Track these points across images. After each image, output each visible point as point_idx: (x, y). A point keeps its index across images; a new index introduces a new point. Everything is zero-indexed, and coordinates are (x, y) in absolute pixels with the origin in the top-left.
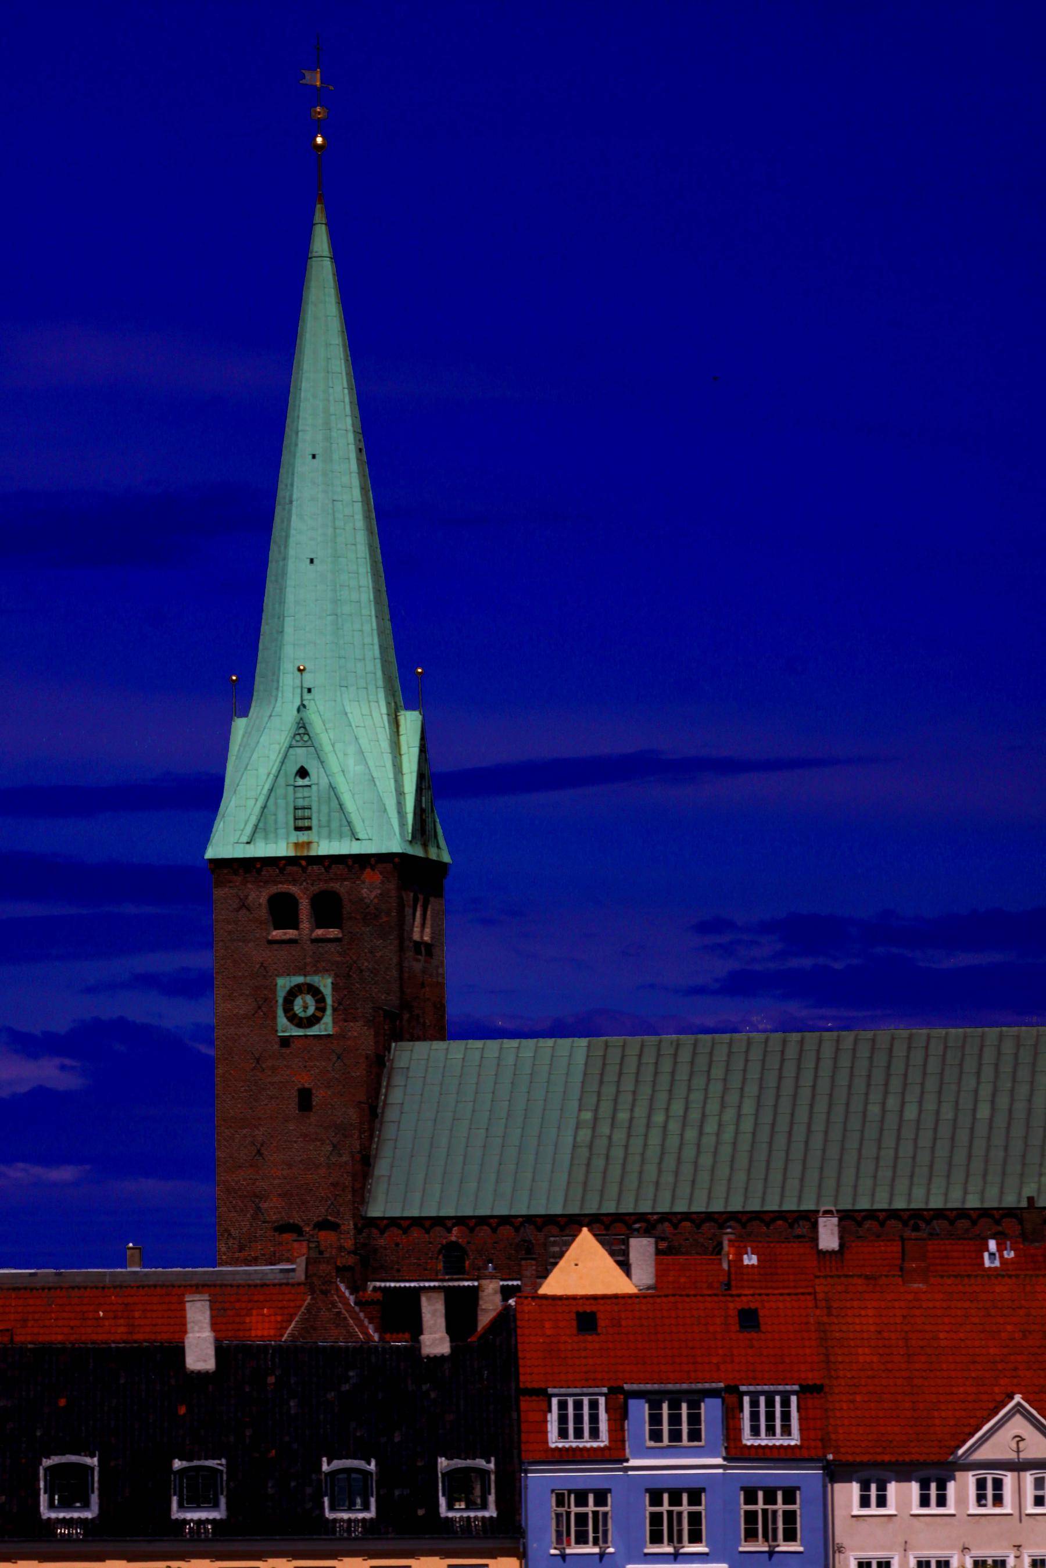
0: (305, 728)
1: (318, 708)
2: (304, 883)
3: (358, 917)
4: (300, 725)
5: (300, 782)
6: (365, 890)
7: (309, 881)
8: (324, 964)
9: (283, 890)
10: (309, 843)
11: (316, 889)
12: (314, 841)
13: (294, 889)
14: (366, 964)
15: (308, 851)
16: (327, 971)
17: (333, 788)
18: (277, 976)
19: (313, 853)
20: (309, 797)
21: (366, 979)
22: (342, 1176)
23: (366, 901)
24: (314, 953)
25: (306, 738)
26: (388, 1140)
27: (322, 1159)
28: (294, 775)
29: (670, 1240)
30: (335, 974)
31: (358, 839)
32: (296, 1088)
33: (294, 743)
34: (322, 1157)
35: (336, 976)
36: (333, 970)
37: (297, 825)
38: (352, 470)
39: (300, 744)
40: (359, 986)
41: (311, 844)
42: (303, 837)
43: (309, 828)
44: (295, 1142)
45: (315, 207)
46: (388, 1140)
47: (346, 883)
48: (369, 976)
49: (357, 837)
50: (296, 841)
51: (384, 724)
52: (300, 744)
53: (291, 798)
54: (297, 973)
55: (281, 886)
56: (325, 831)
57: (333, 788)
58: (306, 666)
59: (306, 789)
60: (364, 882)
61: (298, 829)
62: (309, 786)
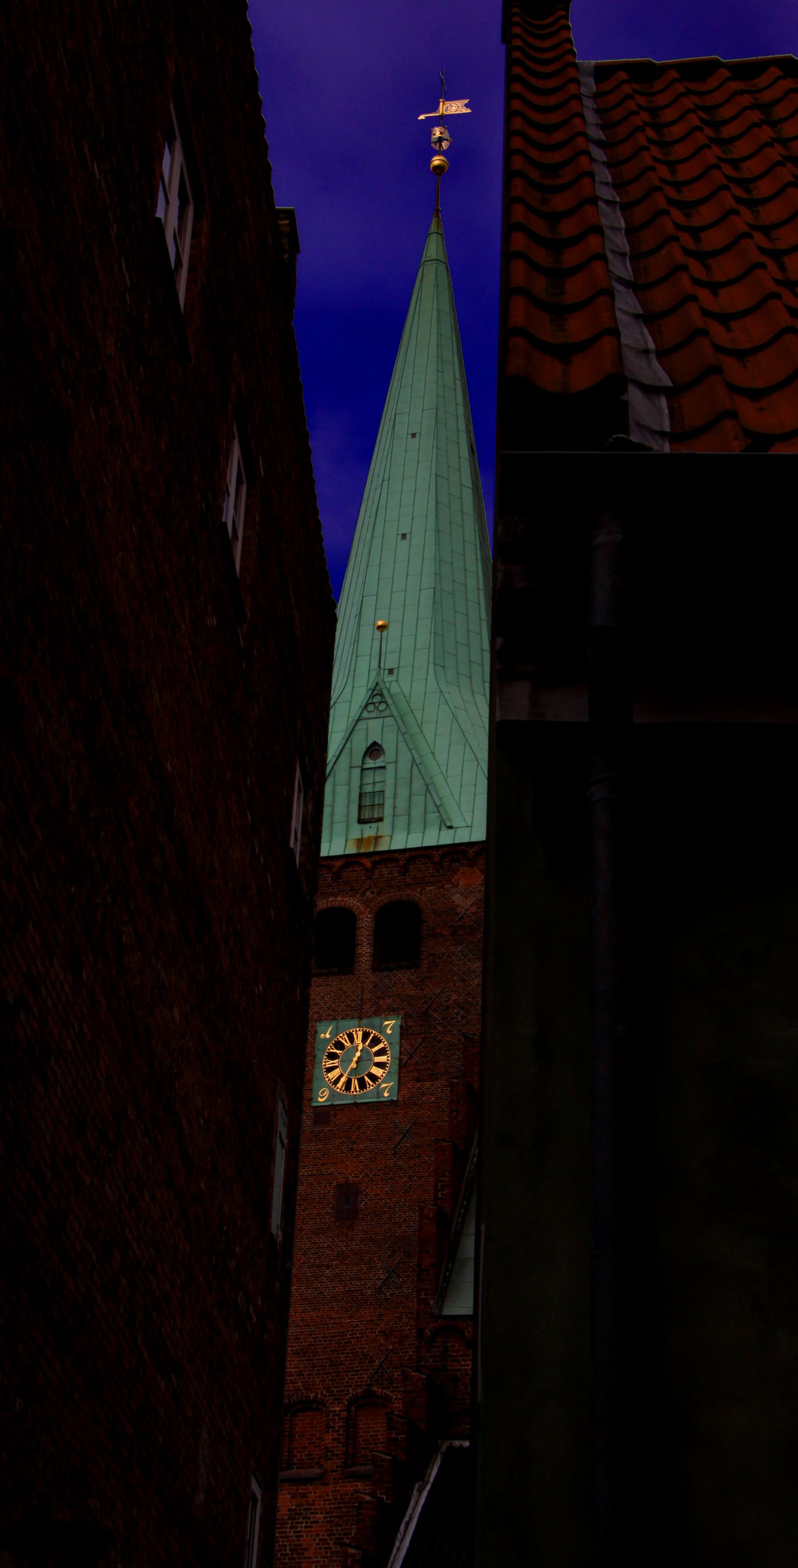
0: (381, 695)
1: (401, 689)
2: (368, 893)
3: (444, 933)
4: (375, 692)
5: (370, 763)
6: (456, 896)
7: (375, 890)
8: (389, 1001)
9: (336, 904)
10: (377, 838)
11: (384, 899)
12: (383, 835)
13: (352, 902)
14: (454, 997)
15: (375, 846)
16: (394, 1010)
17: (455, 717)
18: (317, 1021)
19: (383, 847)
20: (384, 781)
21: (453, 1018)
22: (401, 1318)
23: (458, 910)
24: (375, 987)
25: (382, 707)
26: (365, 784)
27: (369, 1292)
28: (362, 754)
29: (462, 906)
30: (406, 1014)
31: (451, 827)
32: (335, 1183)
33: (365, 714)
34: (369, 1288)
35: (406, 1018)
36: (403, 1009)
37: (362, 817)
38: (460, 428)
39: (374, 715)
40: (441, 1030)
41: (380, 839)
42: (369, 831)
43: (380, 820)
44: (328, 1267)
45: (432, 219)
46: (365, 784)
47: (428, 888)
48: (457, 1014)
49: (448, 824)
50: (359, 837)
51: (485, 693)
52: (374, 715)
53: (356, 783)
54: (348, 1015)
55: (331, 899)
56: (402, 821)
57: (455, 717)
58: (391, 628)
59: (378, 772)
60: (456, 886)
61: (361, 821)
62: (384, 767)
